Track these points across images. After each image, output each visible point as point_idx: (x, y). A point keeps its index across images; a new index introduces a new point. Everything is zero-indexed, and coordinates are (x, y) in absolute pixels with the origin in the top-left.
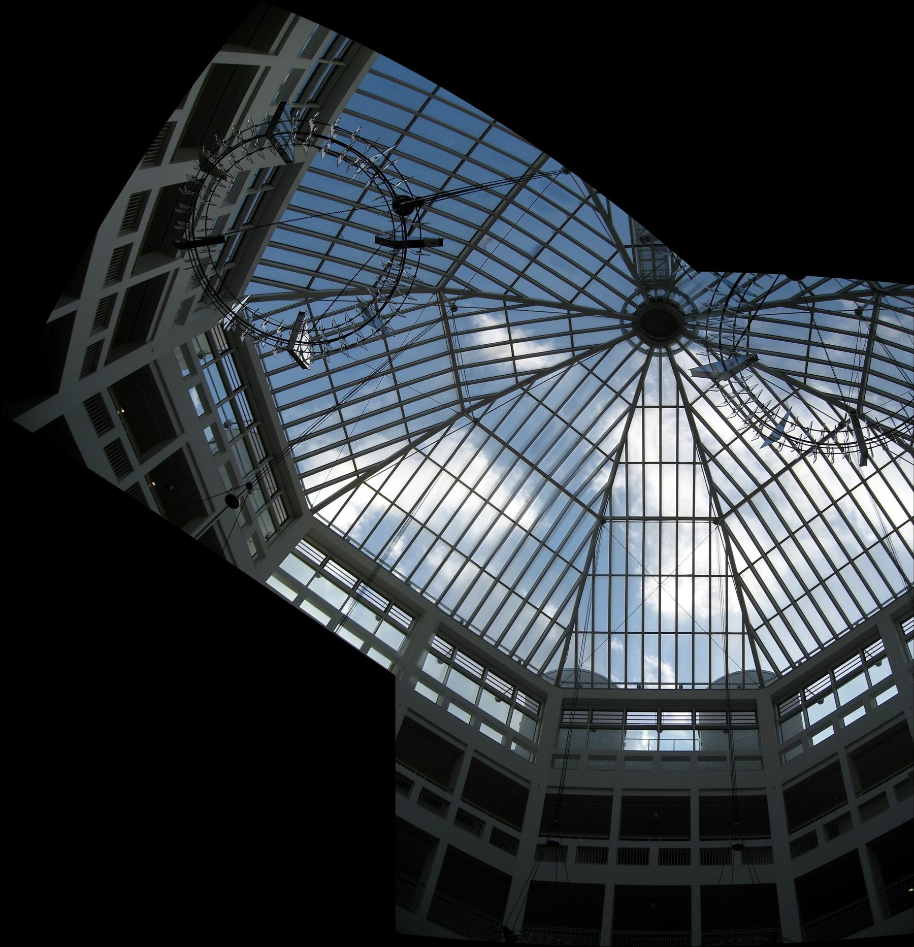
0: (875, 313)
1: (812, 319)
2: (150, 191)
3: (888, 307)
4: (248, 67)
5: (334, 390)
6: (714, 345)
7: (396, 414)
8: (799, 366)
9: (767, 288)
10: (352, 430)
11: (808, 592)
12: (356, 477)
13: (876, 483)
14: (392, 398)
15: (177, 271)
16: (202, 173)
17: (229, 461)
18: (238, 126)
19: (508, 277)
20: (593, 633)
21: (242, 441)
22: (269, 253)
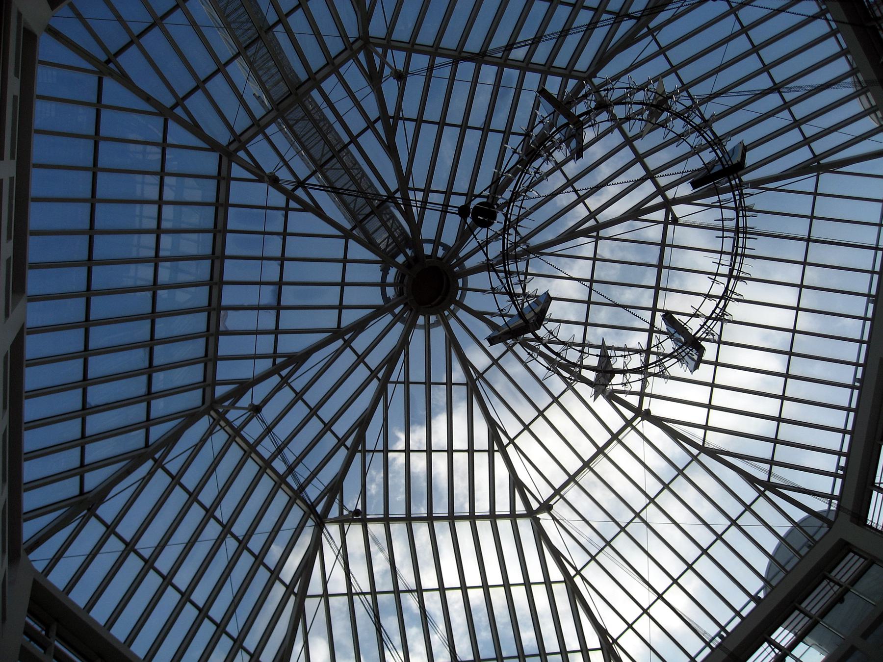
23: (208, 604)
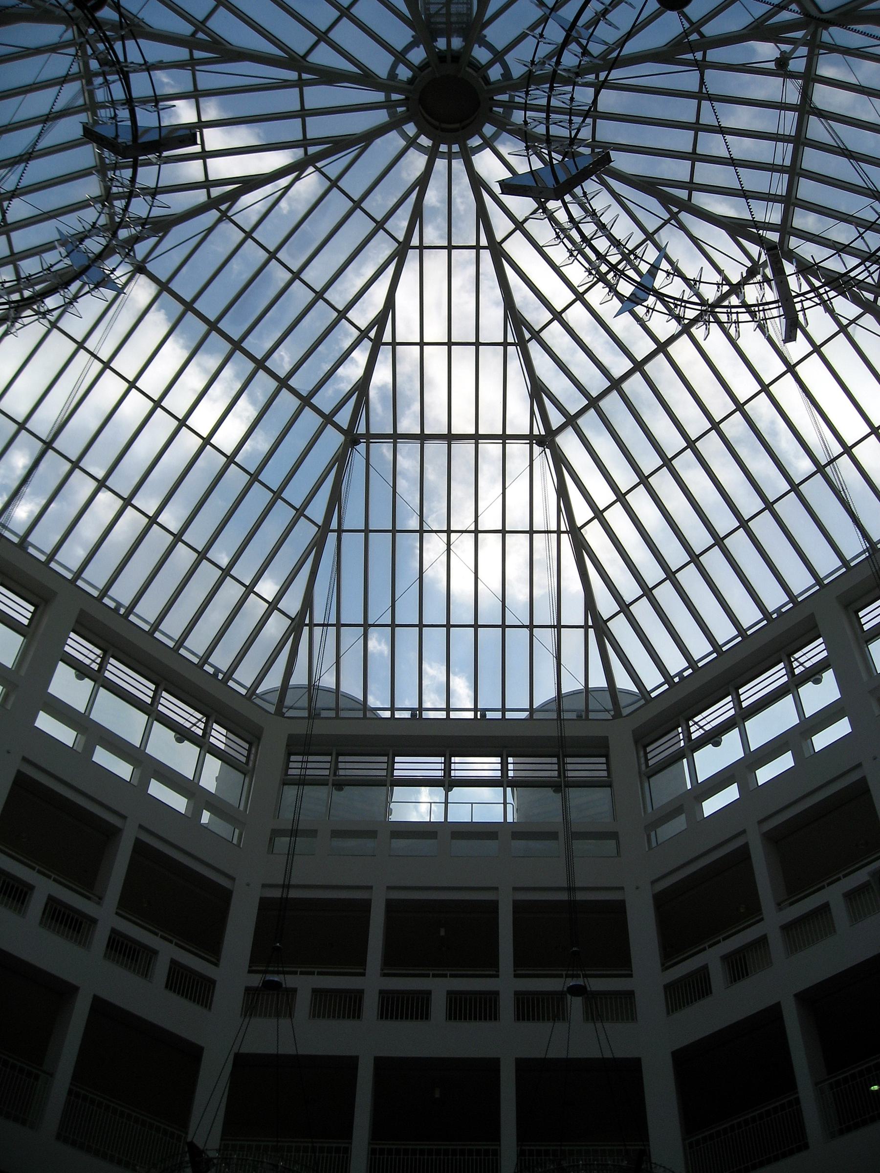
0: (811, 62)
1: (702, 82)
3: (834, 49)
6: (536, 138)
8: (678, 170)
9: (626, 28)
11: (695, 558)
13: (813, 372)
20: (339, 625)
23: (16, 225)
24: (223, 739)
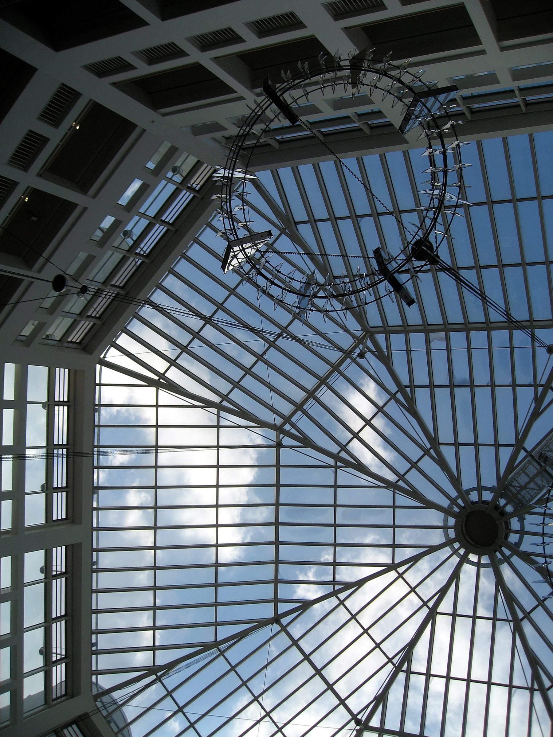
2: (304, 26)
4: (475, 35)
5: (220, 306)
7: (235, 373)
10: (197, 346)
12: (157, 378)
14: (248, 360)
15: (241, 98)
16: (347, 63)
17: (94, 257)
18: (411, 65)
19: (421, 378)
21: (121, 256)
22: (306, 170)
24: (59, 681)
